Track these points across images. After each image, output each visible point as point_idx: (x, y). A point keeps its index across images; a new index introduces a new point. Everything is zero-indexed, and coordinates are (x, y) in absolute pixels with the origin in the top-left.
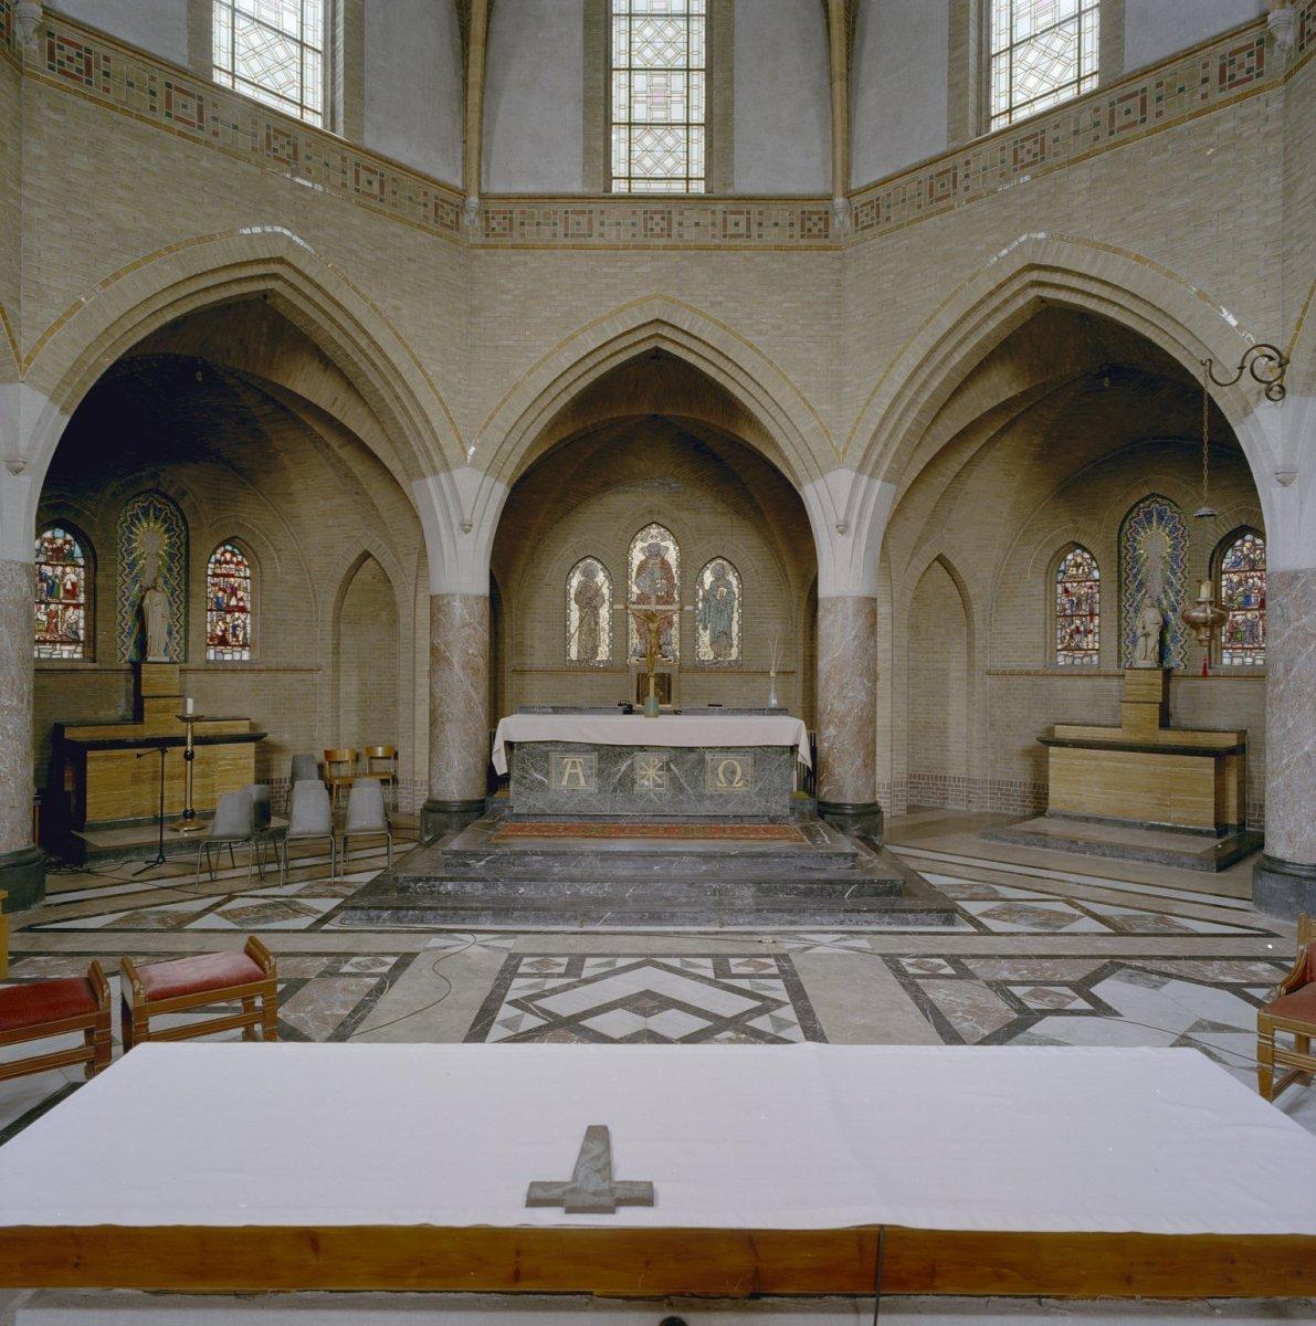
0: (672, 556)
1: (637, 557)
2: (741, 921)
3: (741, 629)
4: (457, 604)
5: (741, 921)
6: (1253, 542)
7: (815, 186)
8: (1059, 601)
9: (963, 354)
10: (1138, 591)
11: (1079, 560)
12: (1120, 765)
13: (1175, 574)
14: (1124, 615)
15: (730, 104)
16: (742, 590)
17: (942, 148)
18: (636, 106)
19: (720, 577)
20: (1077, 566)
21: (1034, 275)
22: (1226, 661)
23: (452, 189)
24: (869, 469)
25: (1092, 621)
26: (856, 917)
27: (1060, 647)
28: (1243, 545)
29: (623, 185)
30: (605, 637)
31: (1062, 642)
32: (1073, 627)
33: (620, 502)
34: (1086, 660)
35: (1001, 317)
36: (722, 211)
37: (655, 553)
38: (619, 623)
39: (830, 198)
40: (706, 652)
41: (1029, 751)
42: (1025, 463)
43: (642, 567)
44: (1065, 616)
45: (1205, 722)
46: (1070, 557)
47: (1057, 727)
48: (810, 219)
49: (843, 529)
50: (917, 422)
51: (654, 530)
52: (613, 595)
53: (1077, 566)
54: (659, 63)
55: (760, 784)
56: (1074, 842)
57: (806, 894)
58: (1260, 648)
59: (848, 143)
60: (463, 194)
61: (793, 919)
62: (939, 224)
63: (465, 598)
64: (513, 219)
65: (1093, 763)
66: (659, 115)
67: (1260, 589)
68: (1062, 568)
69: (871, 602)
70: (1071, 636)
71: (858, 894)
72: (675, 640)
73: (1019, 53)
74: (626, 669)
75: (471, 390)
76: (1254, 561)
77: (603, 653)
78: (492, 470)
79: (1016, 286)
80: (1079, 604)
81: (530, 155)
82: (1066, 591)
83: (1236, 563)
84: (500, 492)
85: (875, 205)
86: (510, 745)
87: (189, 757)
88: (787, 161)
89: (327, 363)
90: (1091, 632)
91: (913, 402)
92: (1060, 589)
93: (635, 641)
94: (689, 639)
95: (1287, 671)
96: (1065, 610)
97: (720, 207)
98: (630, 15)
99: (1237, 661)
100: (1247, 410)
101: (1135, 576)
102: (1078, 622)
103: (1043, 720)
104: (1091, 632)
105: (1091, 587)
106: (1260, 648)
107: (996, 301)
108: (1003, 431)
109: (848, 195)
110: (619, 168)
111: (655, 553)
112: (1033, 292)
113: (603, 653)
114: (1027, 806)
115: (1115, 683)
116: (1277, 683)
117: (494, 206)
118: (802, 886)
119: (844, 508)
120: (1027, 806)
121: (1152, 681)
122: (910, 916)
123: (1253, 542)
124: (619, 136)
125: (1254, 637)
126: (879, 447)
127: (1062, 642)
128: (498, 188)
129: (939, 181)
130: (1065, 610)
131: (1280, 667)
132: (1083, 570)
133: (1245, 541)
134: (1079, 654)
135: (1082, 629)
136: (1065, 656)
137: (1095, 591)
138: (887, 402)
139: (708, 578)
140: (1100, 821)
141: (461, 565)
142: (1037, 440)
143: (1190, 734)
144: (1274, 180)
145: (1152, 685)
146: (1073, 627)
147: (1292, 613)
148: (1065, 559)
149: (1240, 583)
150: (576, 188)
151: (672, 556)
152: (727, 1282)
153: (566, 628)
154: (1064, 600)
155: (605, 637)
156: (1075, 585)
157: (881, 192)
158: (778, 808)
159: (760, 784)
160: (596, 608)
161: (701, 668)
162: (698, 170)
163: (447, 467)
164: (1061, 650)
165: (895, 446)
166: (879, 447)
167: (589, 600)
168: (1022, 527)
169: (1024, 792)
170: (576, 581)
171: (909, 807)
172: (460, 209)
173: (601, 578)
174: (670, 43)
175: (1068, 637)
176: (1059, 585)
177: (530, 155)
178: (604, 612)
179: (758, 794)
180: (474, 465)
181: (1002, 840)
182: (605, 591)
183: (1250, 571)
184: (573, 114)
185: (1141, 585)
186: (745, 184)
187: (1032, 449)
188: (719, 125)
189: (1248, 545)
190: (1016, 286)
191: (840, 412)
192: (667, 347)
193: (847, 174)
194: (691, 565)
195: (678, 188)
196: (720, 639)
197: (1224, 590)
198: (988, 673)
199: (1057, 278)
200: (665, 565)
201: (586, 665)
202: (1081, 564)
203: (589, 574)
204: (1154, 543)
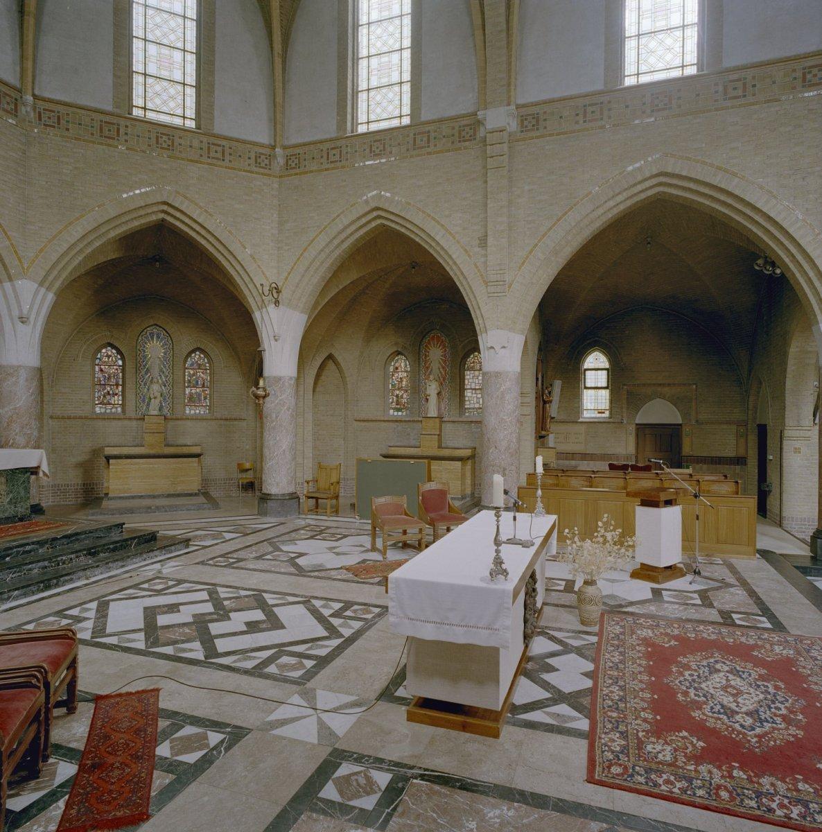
2: (96, 573)
5: (96, 573)
6: (200, 356)
8: (96, 376)
9: (117, 233)
10: (146, 374)
11: (110, 353)
12: (151, 466)
13: (165, 367)
14: (138, 386)
15: (211, 105)
18: (150, 64)
20: (109, 356)
21: (165, 208)
22: (187, 412)
23: (262, 146)
24: (47, 284)
25: (117, 388)
26: (151, 554)
27: (97, 402)
28: (195, 356)
29: (180, 121)
31: (98, 400)
32: (105, 391)
34: (114, 410)
35: (143, 221)
41: (82, 464)
42: (90, 293)
44: (101, 384)
45: (180, 441)
46: (104, 351)
47: (106, 448)
53: (109, 356)
55: (11, 495)
56: (150, 508)
57: (114, 550)
58: (202, 406)
61: (123, 564)
62: (107, 151)
65: (137, 466)
67: (202, 378)
68: (99, 356)
69: (40, 370)
70: (104, 396)
71: (139, 544)
76: (200, 365)
79: (155, 209)
80: (109, 378)
82: (101, 370)
83: (192, 365)
90: (116, 394)
91: (81, 251)
92: (97, 368)
95: (277, 417)
96: (101, 381)
99: (193, 412)
100: (263, 306)
101: (144, 366)
102: (109, 388)
103: (90, 445)
104: (116, 394)
105: (117, 369)
106: (202, 406)
107: (142, 212)
112: (161, 216)
114: (79, 497)
115: (134, 423)
116: (273, 422)
118: (111, 546)
119: (281, 334)
120: (79, 497)
121: (159, 421)
122: (173, 548)
123: (200, 356)
125: (200, 400)
126: (55, 272)
127: (98, 400)
130: (101, 381)
131: (274, 416)
132: (112, 359)
133: (196, 355)
134: (109, 407)
135: (111, 392)
136: (100, 407)
137: (119, 371)
138: (65, 246)
140: (141, 497)
142: (100, 282)
143: (180, 448)
144: (275, 215)
145: (160, 423)
146: (105, 391)
147: (279, 394)
148: (100, 352)
149: (194, 375)
154: (98, 375)
156: (107, 367)
158: (23, 510)
159: (11, 495)
164: (99, 404)
166: (55, 272)
168: (75, 329)
169: (77, 489)
172: (271, 157)
175: (102, 397)
176: (97, 367)
179: (10, 502)
181: (104, 514)
183: (198, 369)
185: (148, 371)
187: (96, 286)
189: (197, 356)
190: (155, 209)
192: (169, 219)
197: (186, 377)
198: (51, 417)
199: (178, 215)
202: (110, 356)
204: (155, 349)
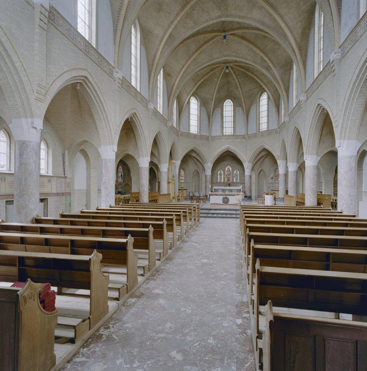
0: (231, 169)
1: (226, 169)
3: (239, 178)
4: (208, 176)
7: (244, 134)
16: (239, 174)
17: (255, 132)
19: (237, 172)
30: (222, 179)
33: (225, 163)
36: (234, 136)
37: (229, 169)
38: (224, 178)
39: (245, 135)
40: (235, 181)
43: (227, 171)
48: (244, 137)
49: (247, 168)
50: (254, 158)
51: (228, 166)
52: (223, 174)
54: (228, 121)
59: (247, 130)
60: (209, 136)
63: (209, 175)
64: (214, 138)
66: (228, 126)
72: (231, 179)
73: (262, 124)
74: (225, 183)
75: (210, 156)
77: (222, 181)
78: (212, 163)
81: (216, 132)
84: (212, 165)
85: (250, 136)
86: (214, 189)
87: (182, 191)
88: (241, 131)
89: (196, 153)
93: (226, 179)
94: (233, 179)
97: (234, 136)
98: (225, 128)
108: (267, 156)
109: (247, 135)
110: (224, 132)
111: (229, 169)
113: (222, 181)
117: (212, 137)
119: (247, 166)
124: (224, 129)
128: (212, 135)
129: (255, 135)
139: (235, 172)
141: (209, 172)
150: (220, 135)
151: (231, 169)
152: (209, 19)
153: (218, 178)
155: (222, 179)
157: (250, 135)
160: (221, 176)
161: (234, 183)
162: (232, 132)
163: (207, 163)
165: (252, 160)
167: (221, 175)
170: (219, 172)
171: (229, 184)
173: (222, 172)
174: (229, 119)
177: (216, 132)
178: (222, 176)
180: (210, 162)
182: (223, 174)
184: (220, 128)
186: (237, 134)
188: (234, 128)
191: (247, 158)
193: (247, 133)
194: (233, 170)
195: (230, 134)
196: (237, 179)
200: (230, 170)
201: (220, 183)
203: (221, 172)
